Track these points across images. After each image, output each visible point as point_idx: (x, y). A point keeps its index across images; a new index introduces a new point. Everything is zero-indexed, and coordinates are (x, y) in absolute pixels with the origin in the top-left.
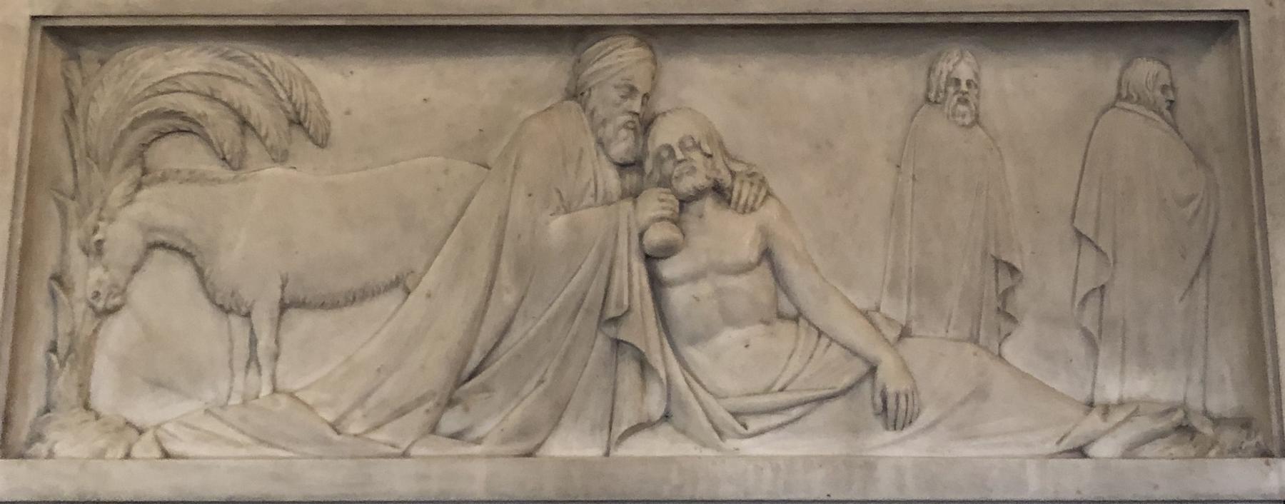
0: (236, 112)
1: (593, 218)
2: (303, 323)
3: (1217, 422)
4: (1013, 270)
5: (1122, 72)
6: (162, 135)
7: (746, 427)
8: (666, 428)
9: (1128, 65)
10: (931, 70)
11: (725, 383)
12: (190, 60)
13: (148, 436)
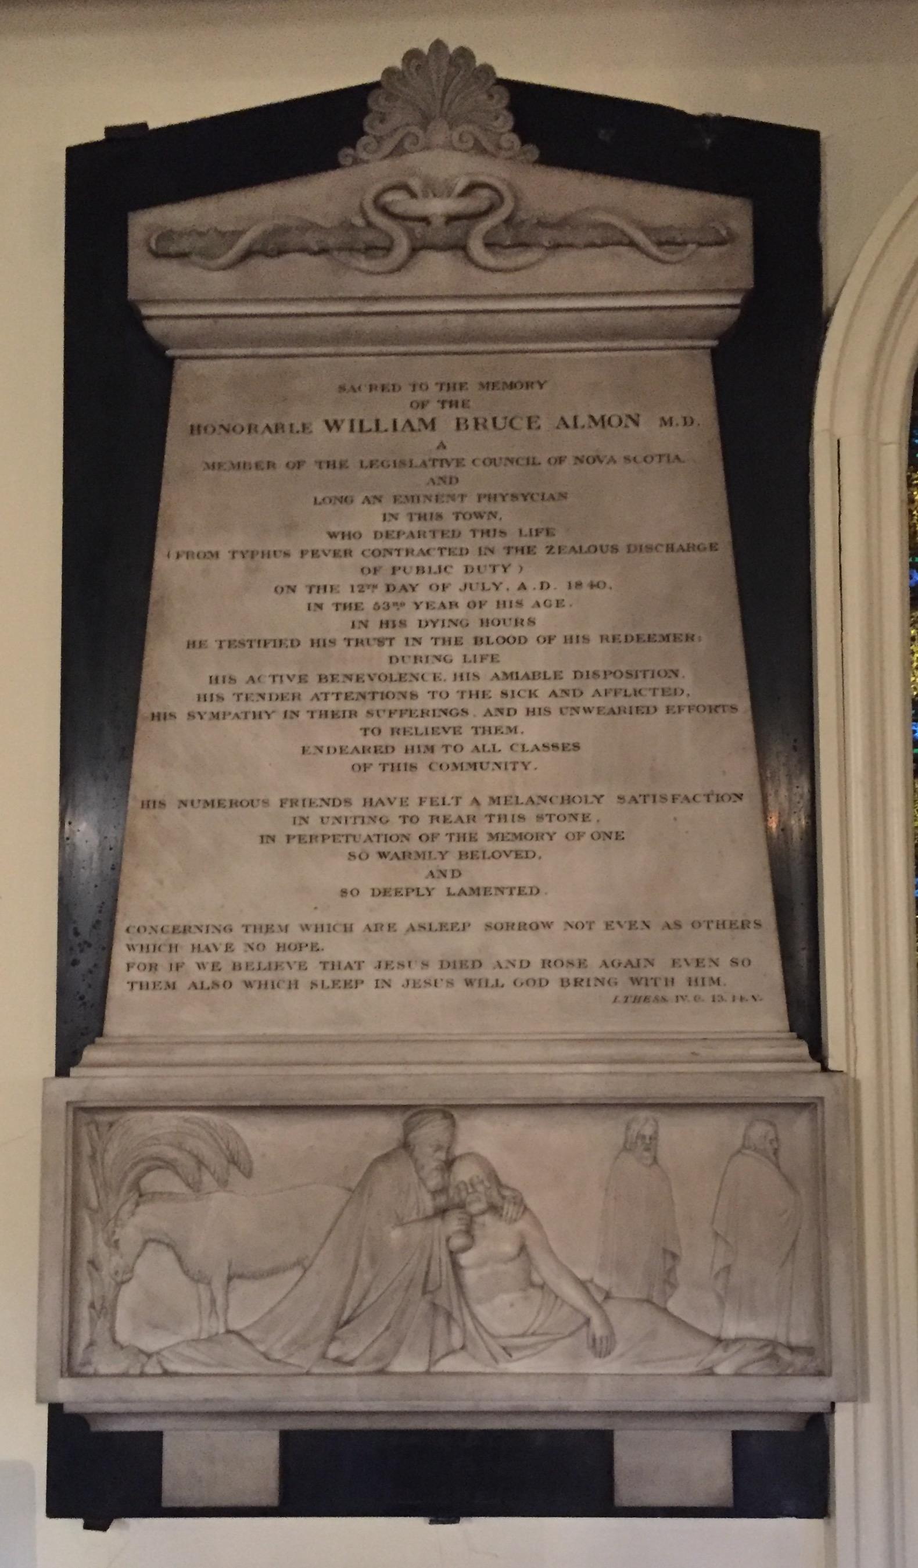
0: (196, 1157)
1: (417, 1231)
2: (241, 1287)
3: (792, 1349)
4: (674, 1256)
5: (747, 1129)
6: (149, 1170)
7: (510, 1356)
8: (463, 1353)
9: (751, 1125)
10: (628, 1128)
11: (498, 1327)
12: (166, 1122)
13: (154, 1359)
